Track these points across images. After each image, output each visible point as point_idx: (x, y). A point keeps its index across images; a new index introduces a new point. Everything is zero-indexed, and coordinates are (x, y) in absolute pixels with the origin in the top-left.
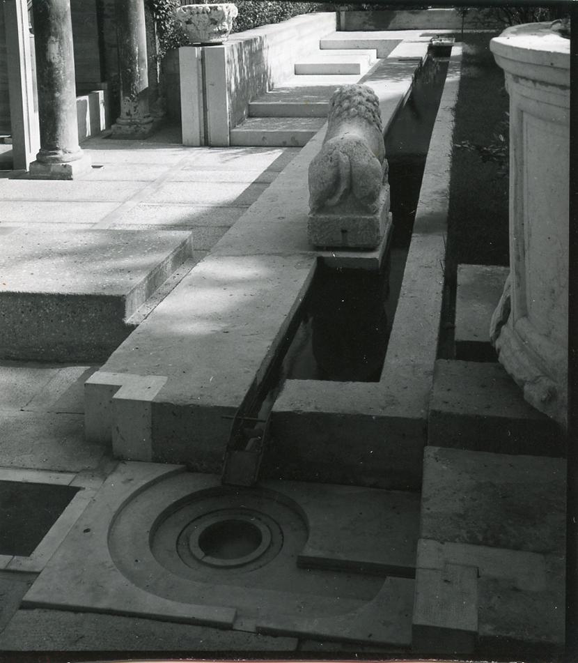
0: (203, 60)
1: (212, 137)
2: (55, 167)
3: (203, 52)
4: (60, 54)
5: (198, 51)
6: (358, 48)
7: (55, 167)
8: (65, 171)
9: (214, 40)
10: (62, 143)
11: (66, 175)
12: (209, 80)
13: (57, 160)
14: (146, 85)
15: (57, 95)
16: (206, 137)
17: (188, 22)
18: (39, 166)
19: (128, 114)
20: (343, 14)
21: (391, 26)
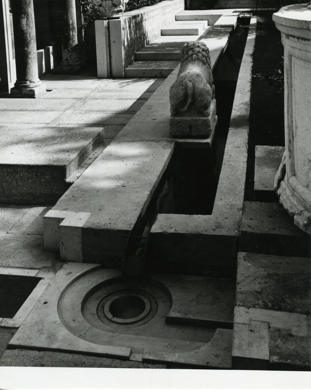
0: (108, 27)
3: (108, 23)
4: (27, 25)
5: (106, 22)
6: (197, 20)
7: (25, 91)
8: (31, 93)
9: (115, 16)
10: (30, 78)
11: (31, 95)
12: (112, 39)
13: (27, 87)
14: (76, 42)
15: (26, 49)
17: (100, 6)
18: (16, 91)
19: (67, 60)
21: (216, 6)
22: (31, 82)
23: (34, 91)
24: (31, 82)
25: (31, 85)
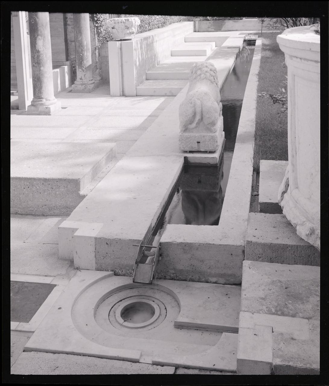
1: (127, 92)
2: (41, 109)
3: (121, 45)
4: (43, 46)
7: (41, 109)
11: (47, 113)
12: (124, 59)
13: (42, 104)
16: (123, 91)
19: (81, 79)
20: (197, 22)
22: (47, 100)
23: (50, 108)
24: (47, 100)
25: (47, 103)
